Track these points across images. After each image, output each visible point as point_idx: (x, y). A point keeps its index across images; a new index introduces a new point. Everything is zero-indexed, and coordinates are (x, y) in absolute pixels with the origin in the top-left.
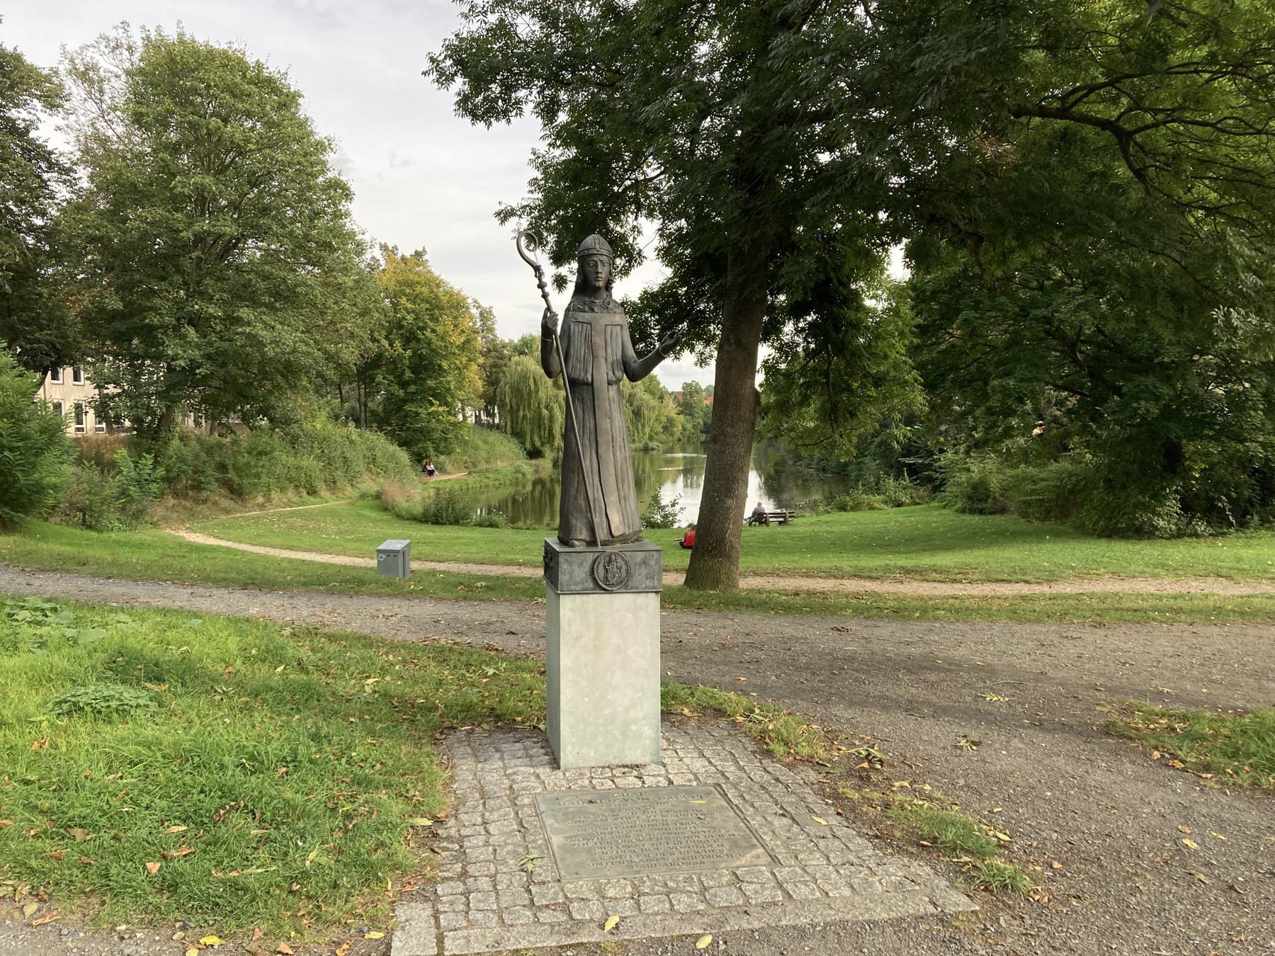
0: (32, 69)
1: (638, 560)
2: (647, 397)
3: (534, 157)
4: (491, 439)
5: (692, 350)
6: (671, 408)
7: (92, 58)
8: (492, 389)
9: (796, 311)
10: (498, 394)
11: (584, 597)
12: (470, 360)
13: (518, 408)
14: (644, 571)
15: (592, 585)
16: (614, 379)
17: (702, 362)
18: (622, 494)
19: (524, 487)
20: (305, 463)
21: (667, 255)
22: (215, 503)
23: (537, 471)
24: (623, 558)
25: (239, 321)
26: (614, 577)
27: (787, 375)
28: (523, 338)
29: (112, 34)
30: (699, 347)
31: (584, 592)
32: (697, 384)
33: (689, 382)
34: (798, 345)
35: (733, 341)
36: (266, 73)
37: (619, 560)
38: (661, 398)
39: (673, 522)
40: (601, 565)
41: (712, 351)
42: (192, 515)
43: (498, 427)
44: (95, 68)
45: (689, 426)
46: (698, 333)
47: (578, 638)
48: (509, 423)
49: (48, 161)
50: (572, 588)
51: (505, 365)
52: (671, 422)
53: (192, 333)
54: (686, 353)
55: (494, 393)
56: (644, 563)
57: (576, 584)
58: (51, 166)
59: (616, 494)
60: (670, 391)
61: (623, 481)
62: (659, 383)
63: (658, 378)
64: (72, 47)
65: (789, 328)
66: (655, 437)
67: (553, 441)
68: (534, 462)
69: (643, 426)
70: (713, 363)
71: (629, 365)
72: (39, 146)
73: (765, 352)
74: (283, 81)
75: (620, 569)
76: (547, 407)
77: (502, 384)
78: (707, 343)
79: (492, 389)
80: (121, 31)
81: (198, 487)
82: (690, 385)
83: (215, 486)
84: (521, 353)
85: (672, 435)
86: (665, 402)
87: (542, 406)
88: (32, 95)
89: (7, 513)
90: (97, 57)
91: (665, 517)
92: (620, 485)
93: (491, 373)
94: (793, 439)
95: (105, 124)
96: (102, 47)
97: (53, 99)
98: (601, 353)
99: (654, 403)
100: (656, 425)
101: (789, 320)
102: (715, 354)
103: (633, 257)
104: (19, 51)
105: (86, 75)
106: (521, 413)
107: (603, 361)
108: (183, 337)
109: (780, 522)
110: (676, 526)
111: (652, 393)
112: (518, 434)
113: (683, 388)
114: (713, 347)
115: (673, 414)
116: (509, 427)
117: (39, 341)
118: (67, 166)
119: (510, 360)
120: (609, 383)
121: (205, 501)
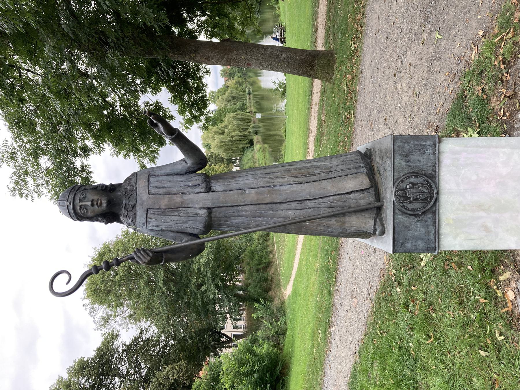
0: (103, 344)
1: (404, 163)
2: (227, 94)
3: (115, 155)
4: (246, 161)
5: (202, 77)
6: (231, 83)
7: (98, 319)
8: (225, 160)
9: (182, 23)
10: (227, 158)
11: (443, 223)
12: (213, 170)
13: (233, 150)
14: (416, 157)
15: (430, 216)
16: (204, 185)
17: (208, 72)
18: (323, 176)
19: (266, 148)
20: (257, 237)
21: (156, 90)
22: (273, 274)
23: (259, 142)
24: (402, 181)
25: (199, 269)
26: (422, 191)
27: (214, 27)
28: (204, 147)
29: (88, 311)
30: (200, 74)
31: (436, 224)
32: (221, 71)
33: (220, 75)
34: (198, 21)
35: (194, 55)
36: (96, 257)
37: (404, 185)
38: (227, 87)
39: (283, 83)
40: (409, 206)
41: (203, 67)
42: (278, 285)
43: (241, 158)
44: (102, 318)
45: (239, 75)
46: (194, 74)
47: (487, 229)
48: (239, 153)
49: (138, 338)
50: (432, 237)
51: (215, 155)
52: (238, 82)
53: (204, 288)
54: (204, 80)
55: (226, 159)
56: (406, 156)
57: (428, 233)
58: (140, 336)
59: (324, 182)
60: (224, 83)
61: (311, 175)
62: (221, 88)
63: (219, 89)
64: (94, 326)
65: (190, 26)
66: (244, 90)
67: (246, 135)
68: (255, 144)
69: (239, 95)
70: (209, 66)
71: (189, 168)
72: (133, 341)
73: (202, 38)
74: (99, 250)
75: (413, 184)
76: (232, 138)
77: (223, 156)
78: (199, 69)
79: (225, 160)
80: (87, 307)
81: (266, 280)
82: (221, 74)
83: (266, 274)
84: (210, 148)
85: (243, 82)
86: (229, 85)
87: (232, 140)
88: (113, 345)
89: (279, 368)
90: (98, 316)
91: (280, 86)
92: (315, 178)
93: (219, 161)
94: (247, 23)
95: (124, 314)
96: (94, 314)
97: (114, 336)
98: (177, 199)
99: (229, 90)
100: (239, 89)
101: (186, 25)
102: (204, 65)
103: (158, 106)
104: (96, 349)
105: (106, 320)
106: (235, 148)
107: (186, 197)
108: (206, 291)
109: (284, 31)
110: (285, 82)
111: (225, 91)
112: (243, 150)
113: (223, 77)
114: (201, 66)
115: (234, 82)
116: (241, 153)
117: (209, 340)
118: (140, 331)
119: (213, 153)
120: (209, 190)
121: (272, 278)
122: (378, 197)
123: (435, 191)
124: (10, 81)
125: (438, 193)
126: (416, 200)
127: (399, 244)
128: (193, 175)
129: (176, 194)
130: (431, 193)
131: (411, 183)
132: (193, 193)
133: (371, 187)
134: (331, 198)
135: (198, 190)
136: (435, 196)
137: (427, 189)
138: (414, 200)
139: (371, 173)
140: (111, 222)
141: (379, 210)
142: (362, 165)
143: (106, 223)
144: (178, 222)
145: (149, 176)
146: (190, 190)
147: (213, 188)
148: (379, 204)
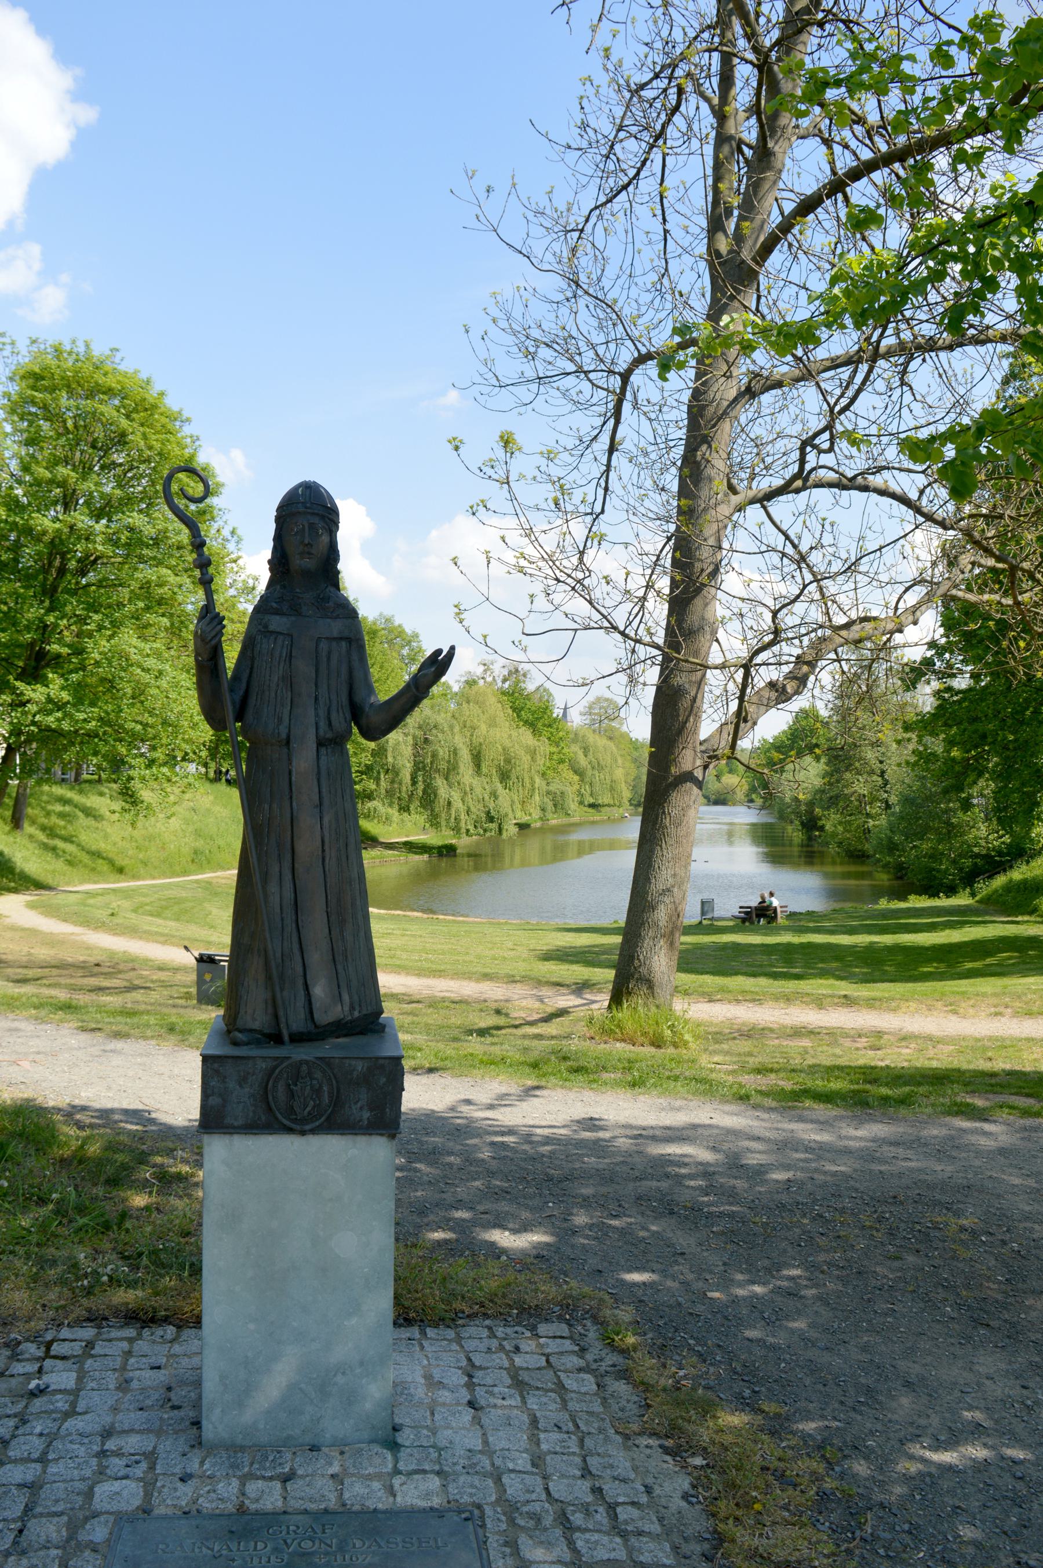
16: (329, 735)
31: (252, 1128)
75: (318, 1092)
122: (298, 1038)
123: (307, 1127)
124: (771, 50)
125: (303, 1133)
126: (291, 1095)
127: (216, 1065)
128: (348, 716)
129: (316, 685)
130: (304, 1121)
131: (321, 1087)
132: (317, 715)
133: (316, 1026)
134: (324, 790)
135: (323, 724)
136: (298, 1127)
137: (309, 1113)
138: (292, 1091)
139: (341, 1028)
140: (271, 569)
141: (276, 1039)
142: (356, 1014)
143: (269, 562)
144: (888, 411)
145: (349, 640)
146: (322, 713)
147: (323, 750)
148: (286, 1038)
